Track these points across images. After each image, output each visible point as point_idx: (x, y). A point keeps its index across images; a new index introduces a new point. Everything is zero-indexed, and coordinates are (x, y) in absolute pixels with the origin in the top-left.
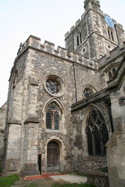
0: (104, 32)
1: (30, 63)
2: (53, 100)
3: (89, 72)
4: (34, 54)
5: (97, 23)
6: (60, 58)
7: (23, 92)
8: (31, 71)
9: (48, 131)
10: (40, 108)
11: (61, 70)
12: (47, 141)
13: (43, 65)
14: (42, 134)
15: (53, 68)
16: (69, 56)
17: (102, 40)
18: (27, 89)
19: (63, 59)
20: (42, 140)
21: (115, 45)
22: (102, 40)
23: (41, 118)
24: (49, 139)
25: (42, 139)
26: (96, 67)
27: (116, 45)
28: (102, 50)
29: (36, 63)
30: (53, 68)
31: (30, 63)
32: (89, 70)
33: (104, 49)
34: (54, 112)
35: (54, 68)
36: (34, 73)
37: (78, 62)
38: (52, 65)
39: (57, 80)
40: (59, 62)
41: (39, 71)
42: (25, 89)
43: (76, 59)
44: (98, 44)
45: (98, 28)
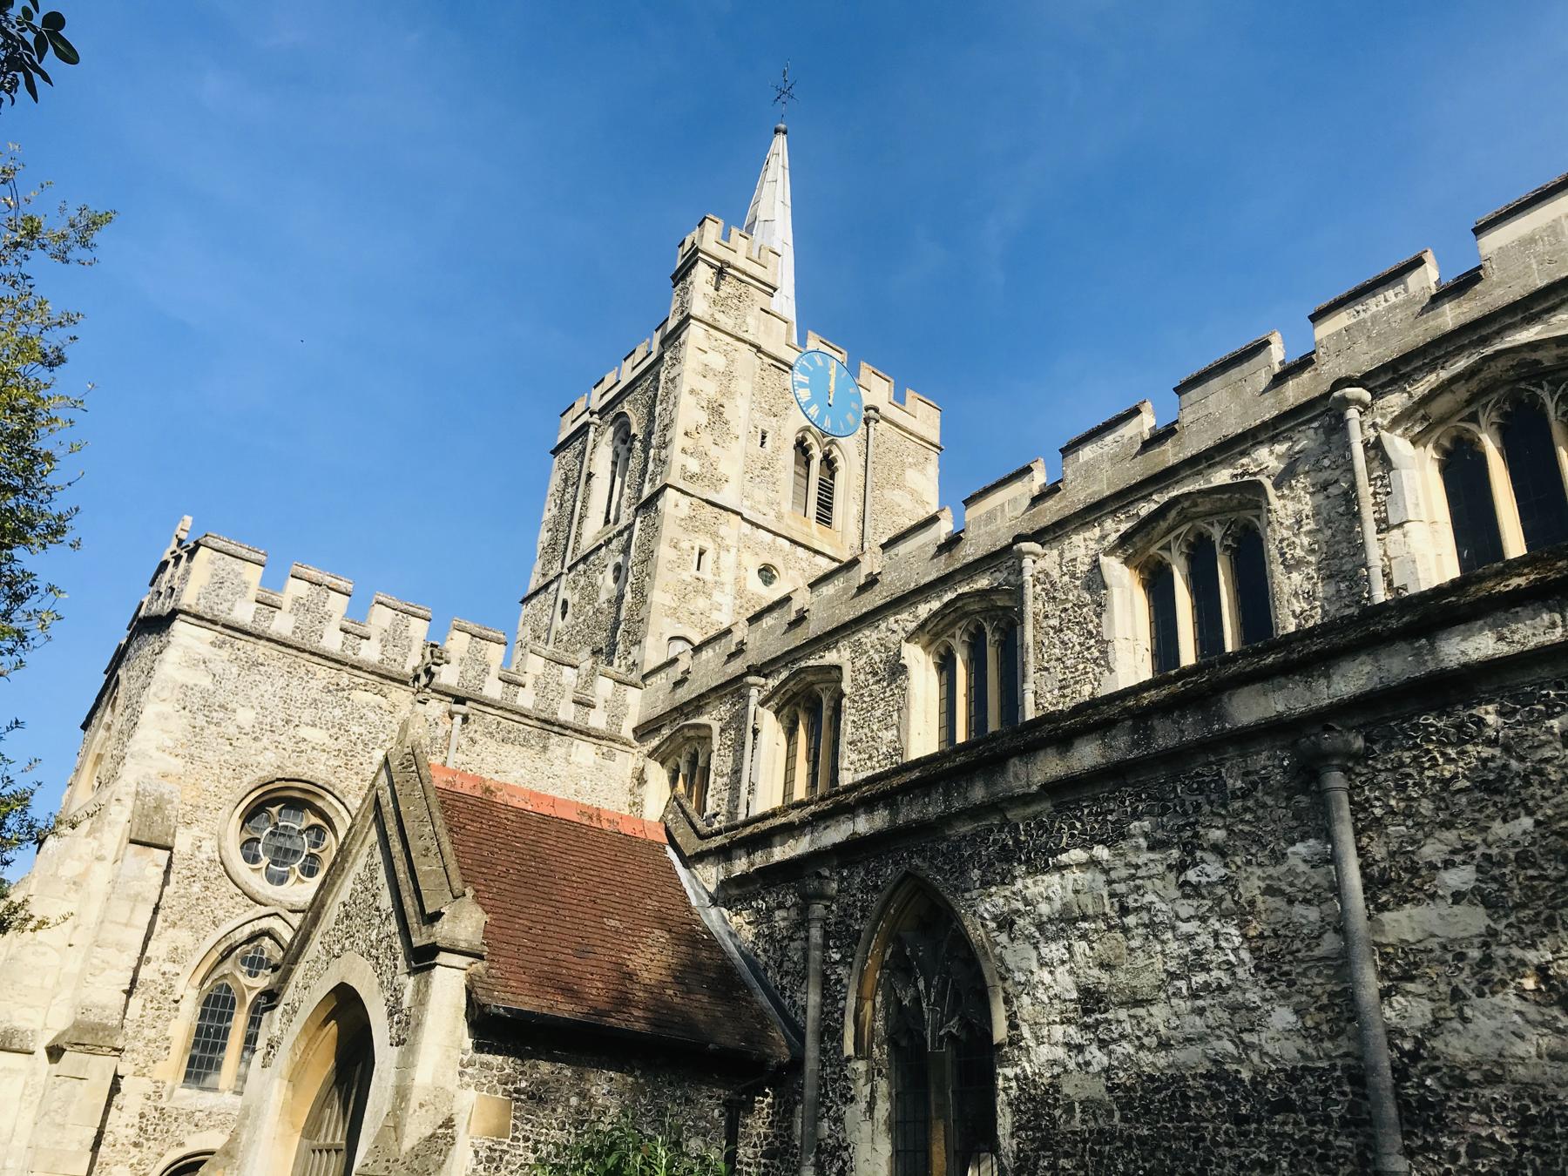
0: (760, 472)
1: (167, 708)
2: (264, 924)
3: (560, 752)
4: (206, 651)
5: (716, 410)
6: (372, 673)
7: (86, 873)
8: (159, 754)
9: (191, 1098)
10: (168, 967)
11: (360, 746)
12: (161, 1155)
13: (246, 717)
14: (142, 1116)
15: (305, 732)
16: (584, 704)
17: (715, 535)
18: (111, 858)
19: (551, 725)
20: (134, 1151)
21: (819, 559)
22: (715, 535)
23: (159, 1024)
24: (181, 1144)
25: (136, 1145)
26: (615, 718)
27: (834, 560)
28: (701, 603)
29: (206, 708)
30: (305, 732)
31: (167, 708)
32: (555, 739)
33: (717, 596)
34: (251, 989)
35: (317, 736)
36: (177, 765)
37: (493, 689)
38: (307, 715)
39: (320, 803)
40: (359, 696)
41: (209, 756)
42: (100, 859)
43: (486, 671)
44: (680, 564)
45: (714, 452)
